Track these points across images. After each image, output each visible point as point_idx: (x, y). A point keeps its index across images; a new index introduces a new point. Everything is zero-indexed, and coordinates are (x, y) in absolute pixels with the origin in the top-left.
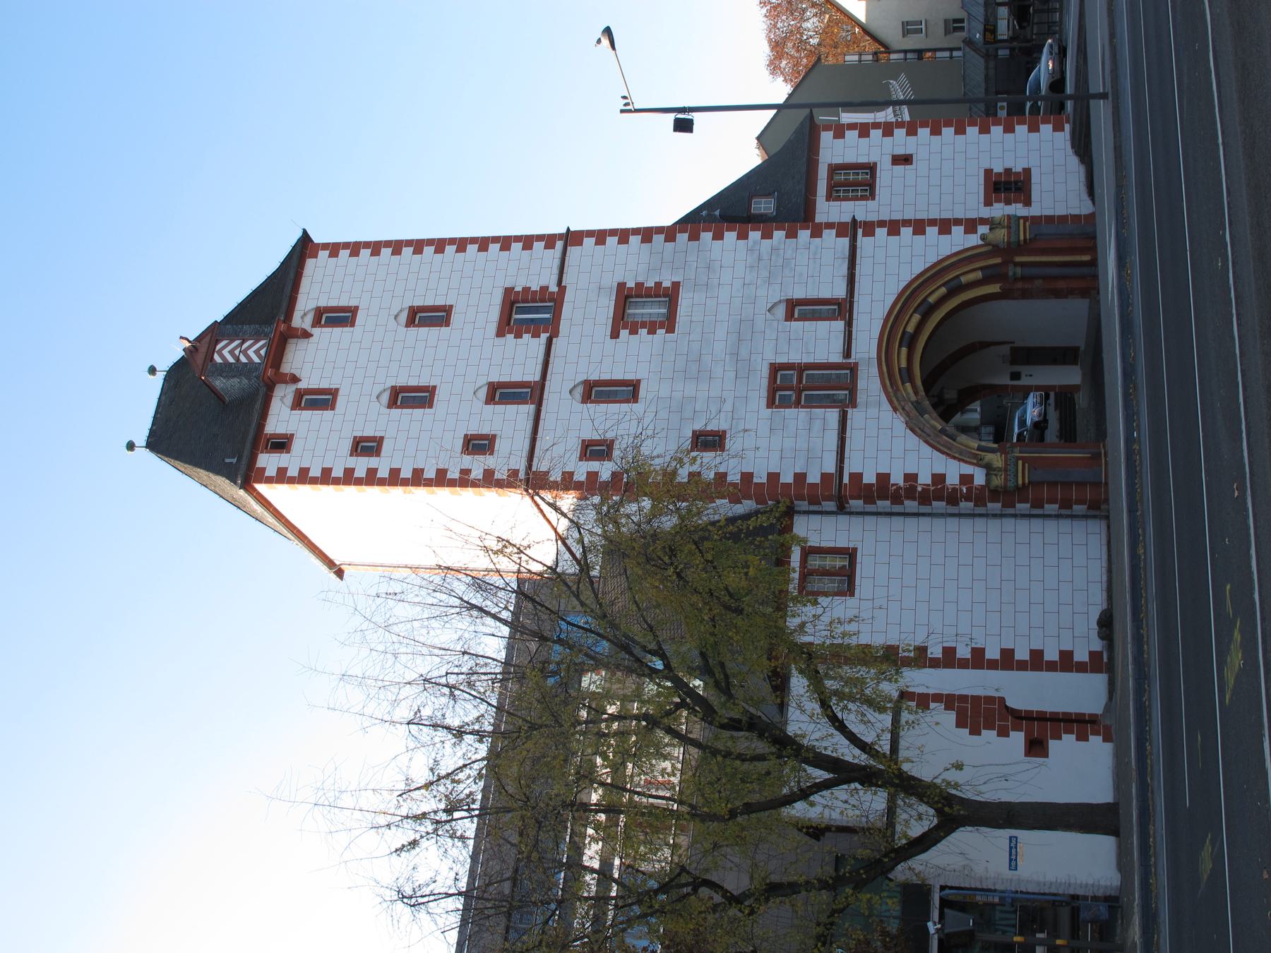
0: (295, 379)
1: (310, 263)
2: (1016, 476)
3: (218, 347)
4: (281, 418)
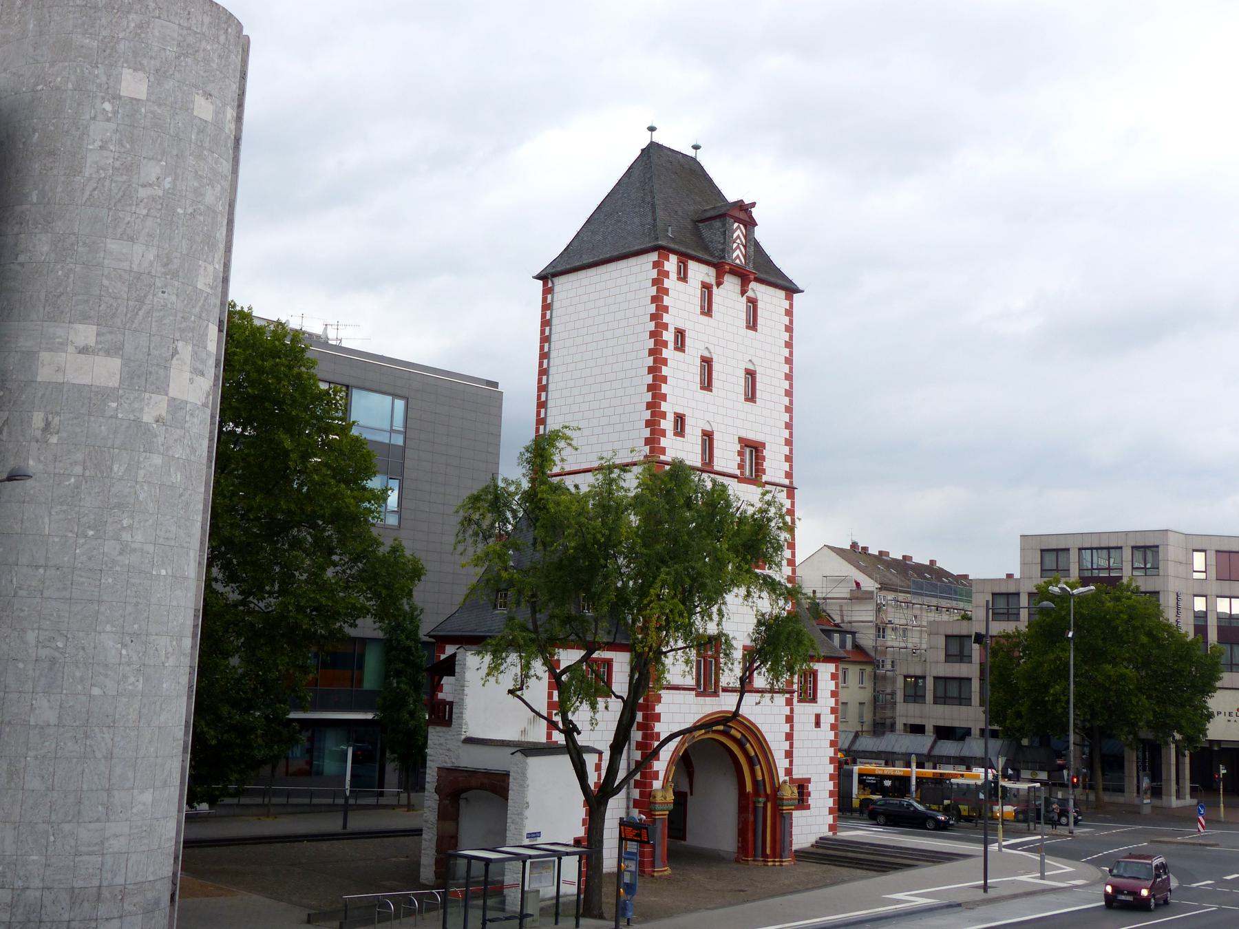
0: (719, 284)
1: (782, 294)
2: (662, 810)
3: (741, 226)
4: (699, 273)
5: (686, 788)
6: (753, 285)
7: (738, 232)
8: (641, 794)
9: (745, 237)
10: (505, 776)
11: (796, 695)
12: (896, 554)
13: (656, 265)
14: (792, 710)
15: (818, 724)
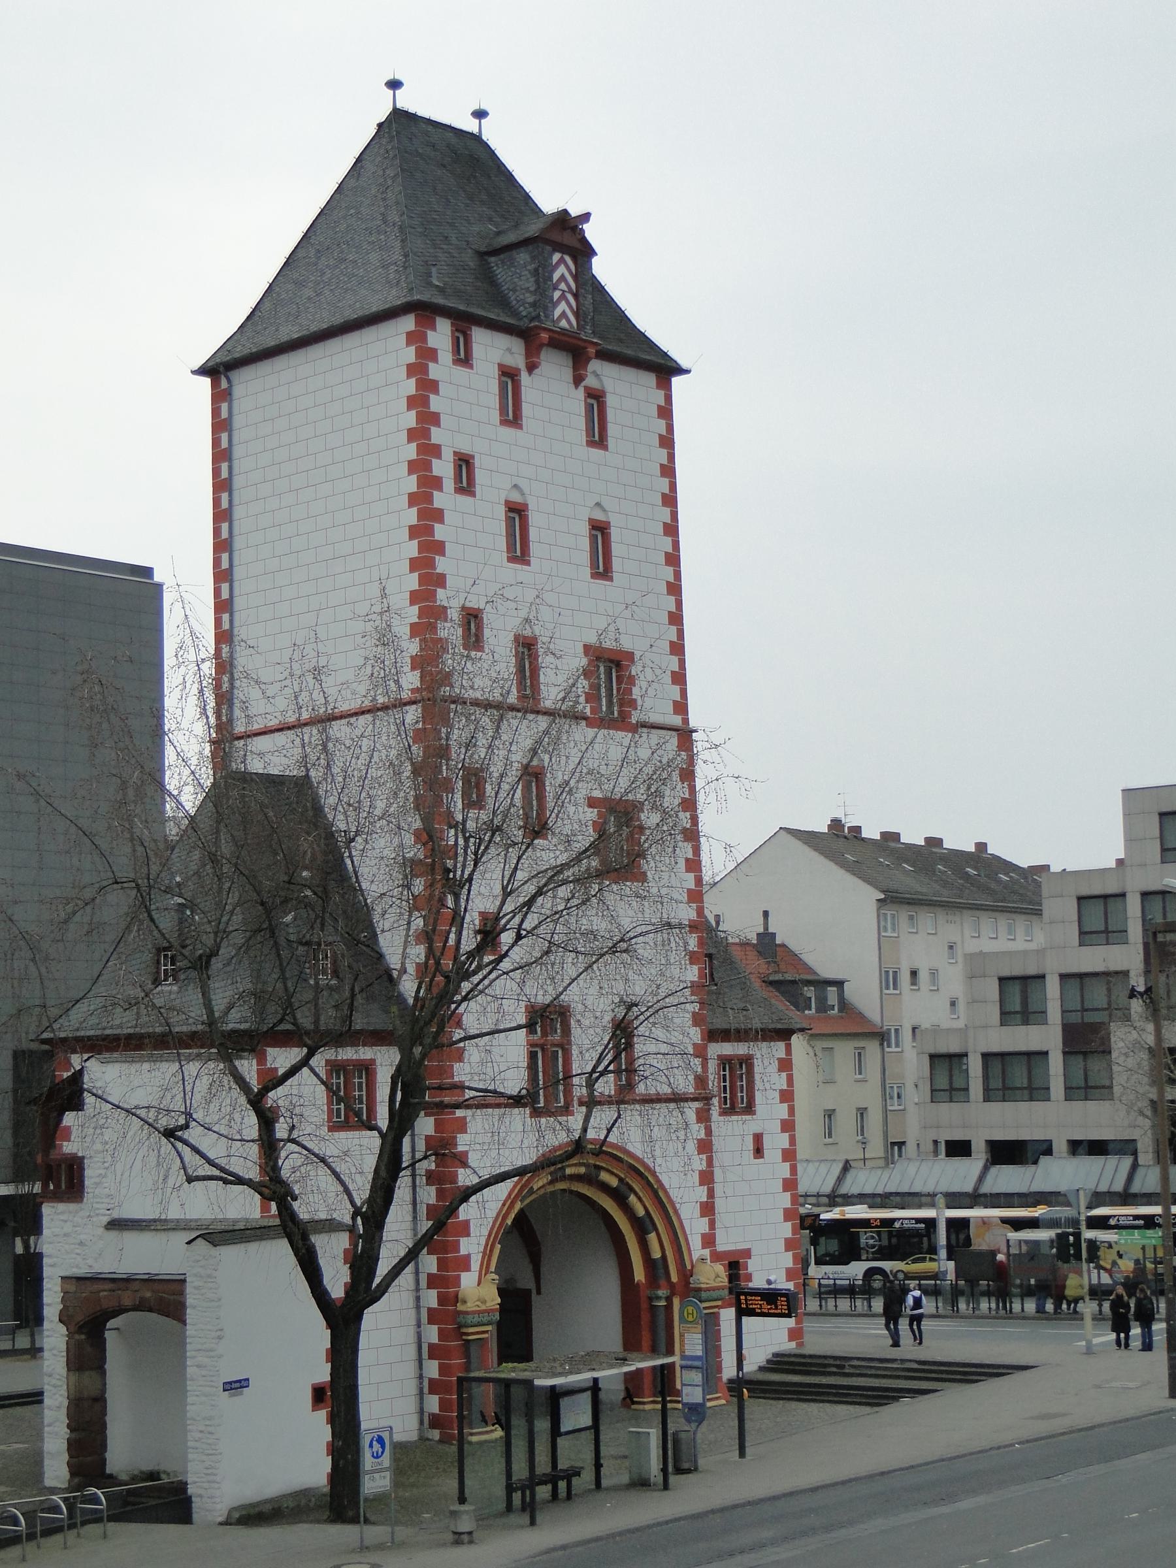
0: (531, 368)
1: (650, 379)
3: (568, 259)
5: (526, 1281)
6: (595, 365)
7: (562, 270)
8: (442, 1300)
9: (576, 278)
10: (178, 1284)
11: (715, 1101)
12: (913, 836)
13: (411, 338)
14: (709, 1132)
15: (758, 1152)
